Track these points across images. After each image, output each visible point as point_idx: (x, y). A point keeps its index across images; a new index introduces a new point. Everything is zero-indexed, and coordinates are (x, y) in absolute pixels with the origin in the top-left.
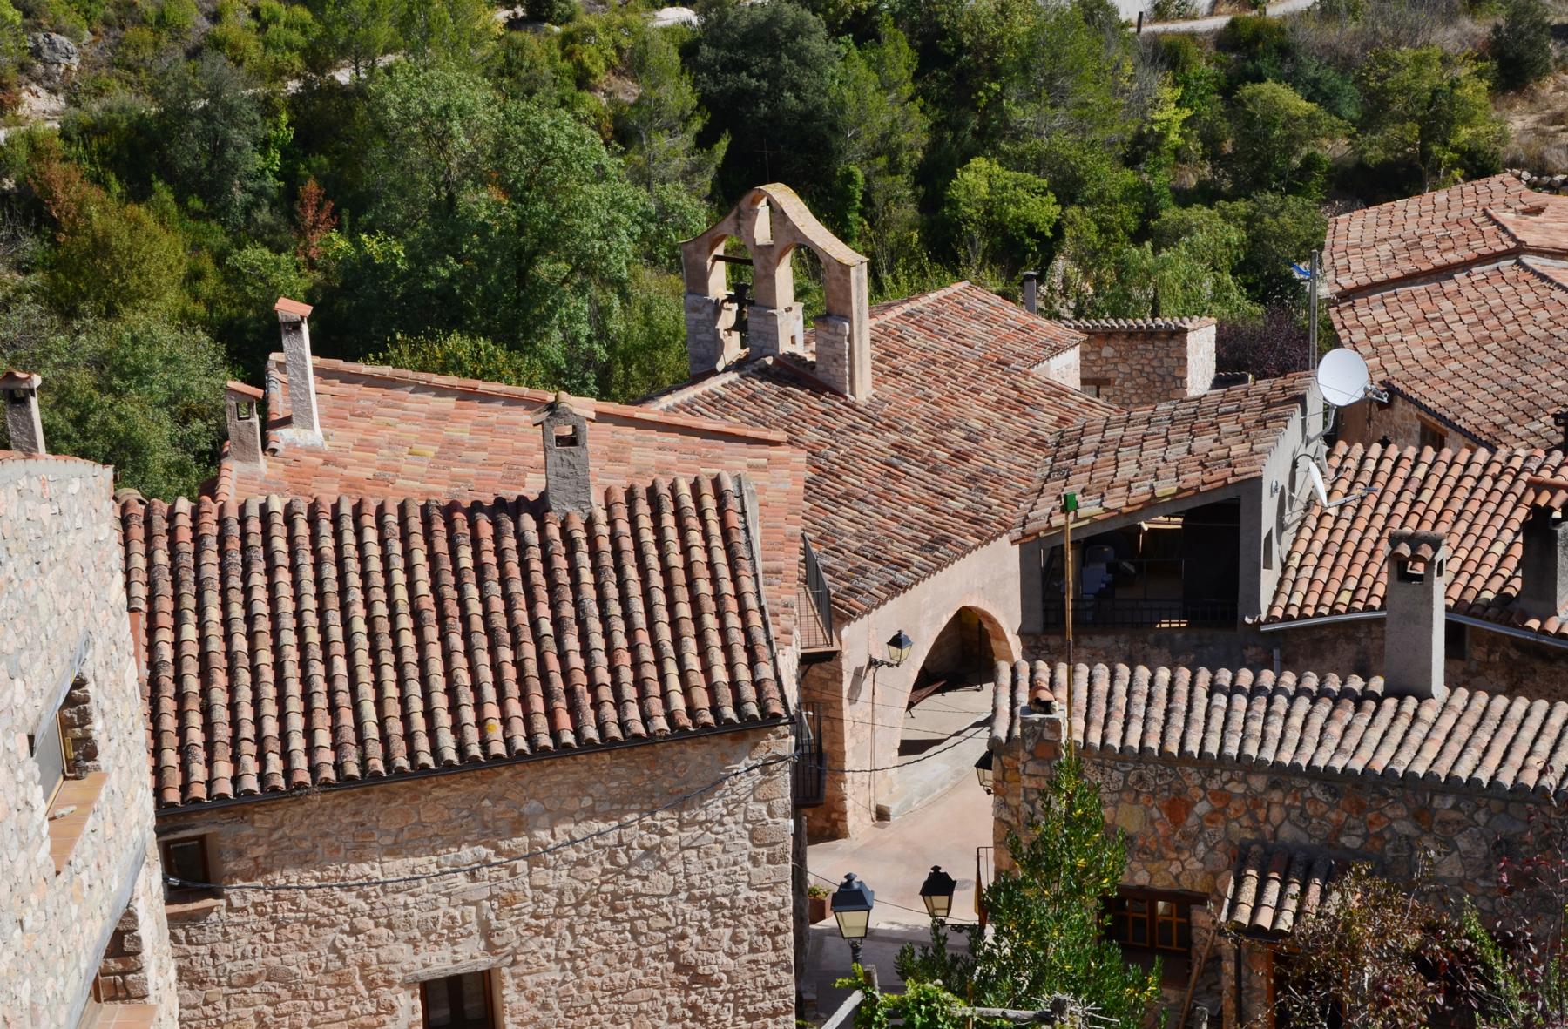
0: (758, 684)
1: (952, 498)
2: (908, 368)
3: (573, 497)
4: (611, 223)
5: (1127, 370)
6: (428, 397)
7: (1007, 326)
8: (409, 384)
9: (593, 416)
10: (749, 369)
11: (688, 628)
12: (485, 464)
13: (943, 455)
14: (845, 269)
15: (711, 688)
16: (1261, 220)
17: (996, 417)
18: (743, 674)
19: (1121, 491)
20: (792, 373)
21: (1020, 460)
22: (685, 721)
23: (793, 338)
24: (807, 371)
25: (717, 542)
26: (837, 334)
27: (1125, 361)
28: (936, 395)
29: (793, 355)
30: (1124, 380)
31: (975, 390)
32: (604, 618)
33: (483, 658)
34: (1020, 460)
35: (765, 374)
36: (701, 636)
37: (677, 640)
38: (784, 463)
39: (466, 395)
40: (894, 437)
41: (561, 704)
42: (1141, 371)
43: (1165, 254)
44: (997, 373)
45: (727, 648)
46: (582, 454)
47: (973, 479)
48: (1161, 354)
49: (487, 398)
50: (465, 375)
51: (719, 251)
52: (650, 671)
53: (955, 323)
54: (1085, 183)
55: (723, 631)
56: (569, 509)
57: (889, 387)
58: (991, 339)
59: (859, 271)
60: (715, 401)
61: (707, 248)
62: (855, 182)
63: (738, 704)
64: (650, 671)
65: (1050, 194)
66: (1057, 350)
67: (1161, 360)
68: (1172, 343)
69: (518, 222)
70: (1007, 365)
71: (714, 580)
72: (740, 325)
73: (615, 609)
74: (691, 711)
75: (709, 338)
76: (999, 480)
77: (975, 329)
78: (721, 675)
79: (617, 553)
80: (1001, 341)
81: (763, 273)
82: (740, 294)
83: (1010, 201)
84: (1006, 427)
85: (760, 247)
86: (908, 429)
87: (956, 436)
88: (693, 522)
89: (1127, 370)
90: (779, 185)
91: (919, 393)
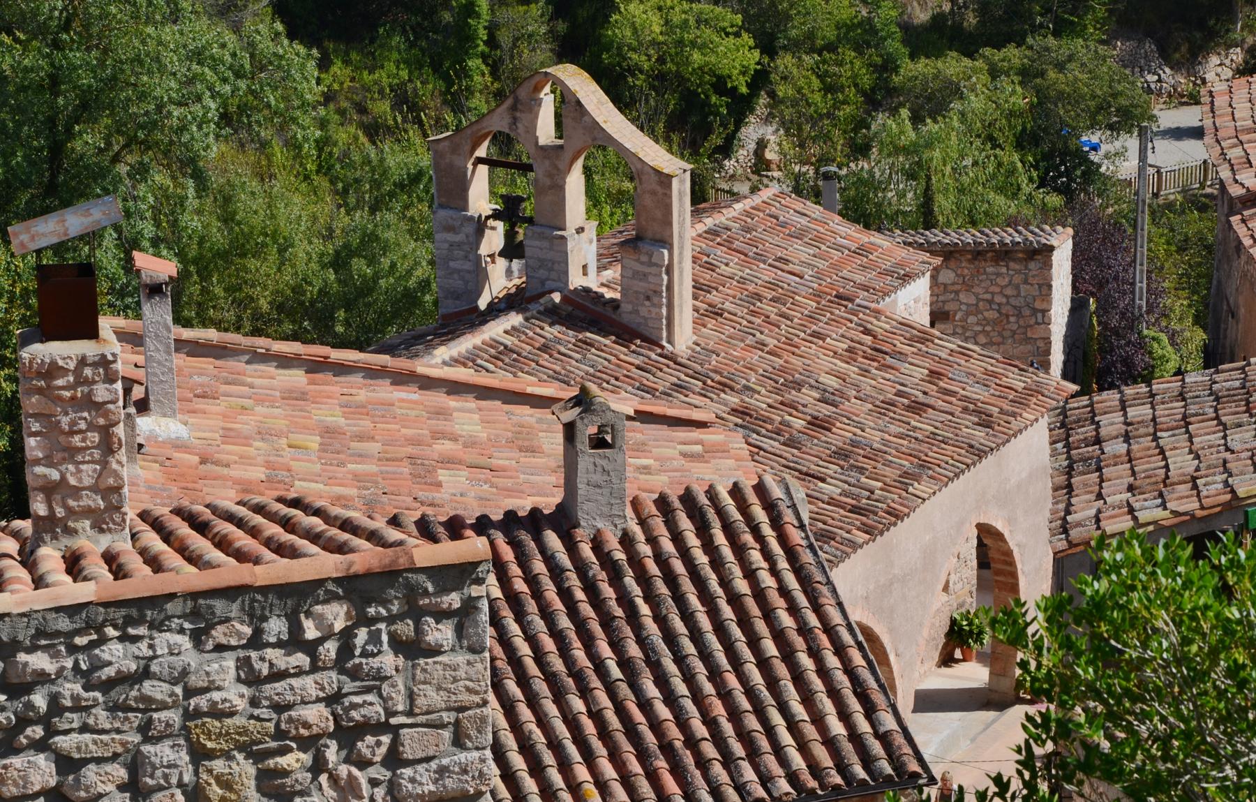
0: (884, 738)
1: (823, 480)
2: (727, 305)
3: (605, 509)
4: (190, 81)
5: (972, 300)
6: (270, 369)
7: (839, 248)
8: (243, 352)
9: (632, 413)
10: (534, 308)
11: (781, 670)
12: (384, 459)
13: (798, 423)
14: (665, 180)
15: (830, 743)
16: (1042, 74)
17: (852, 370)
18: (864, 726)
19: (1184, 489)
20: (587, 314)
21: (894, 429)
22: (812, 784)
23: (585, 267)
24: (609, 311)
25: (783, 564)
26: (651, 264)
27: (969, 288)
28: (772, 342)
29: (587, 290)
30: (968, 314)
31: (816, 335)
32: (680, 660)
33: (551, 709)
34: (894, 429)
35: (553, 315)
36: (798, 678)
37: (772, 683)
38: (722, 450)
39: (315, 367)
40: (733, 400)
41: (661, 764)
42: (990, 302)
43: (930, 126)
44: (839, 312)
45: (834, 693)
46: (619, 458)
47: (841, 454)
48: (1017, 279)
49: (342, 369)
50: (226, 330)
51: (481, 152)
52: (752, 722)
53: (773, 243)
54: (789, 18)
55: (823, 672)
56: (600, 525)
57: (712, 333)
58: (822, 264)
59: (682, 182)
60: (500, 353)
61: (467, 148)
62: (478, 16)
63: (867, 760)
64: (752, 722)
65: (745, 35)
66: (906, 278)
67: (1017, 287)
68: (1032, 265)
69: (50, 76)
70: (851, 301)
71: (793, 609)
72: (512, 250)
73: (689, 647)
74: (815, 769)
75: (468, 266)
76: (874, 455)
77: (799, 252)
78: (837, 728)
79: (671, 579)
80: (836, 267)
81: (548, 182)
82: (509, 210)
83: (693, 44)
84: (867, 384)
85: (542, 148)
86: (747, 388)
87: (808, 396)
88: (748, 538)
89: (972, 300)
90: (571, 68)
91: (750, 340)
